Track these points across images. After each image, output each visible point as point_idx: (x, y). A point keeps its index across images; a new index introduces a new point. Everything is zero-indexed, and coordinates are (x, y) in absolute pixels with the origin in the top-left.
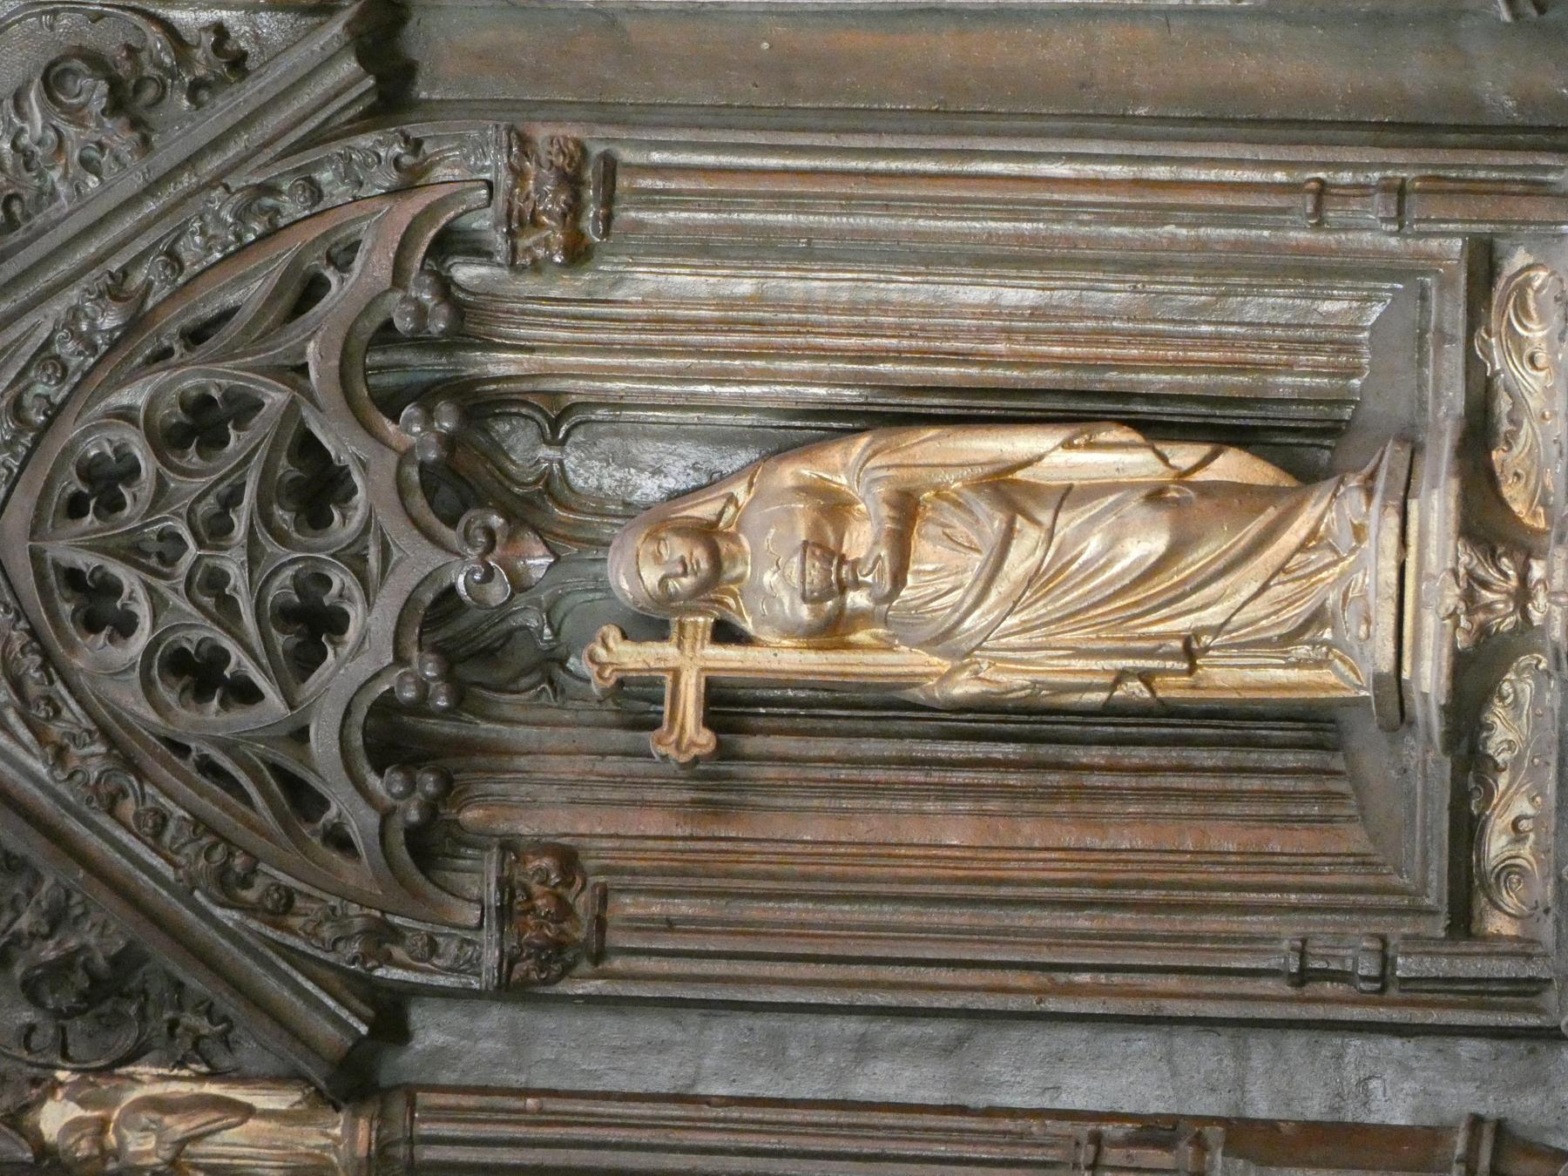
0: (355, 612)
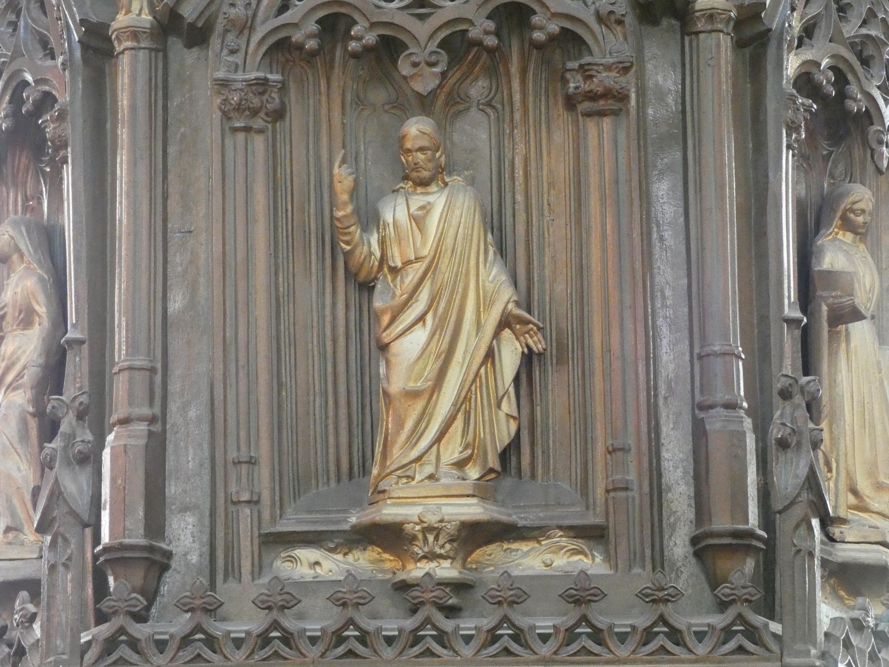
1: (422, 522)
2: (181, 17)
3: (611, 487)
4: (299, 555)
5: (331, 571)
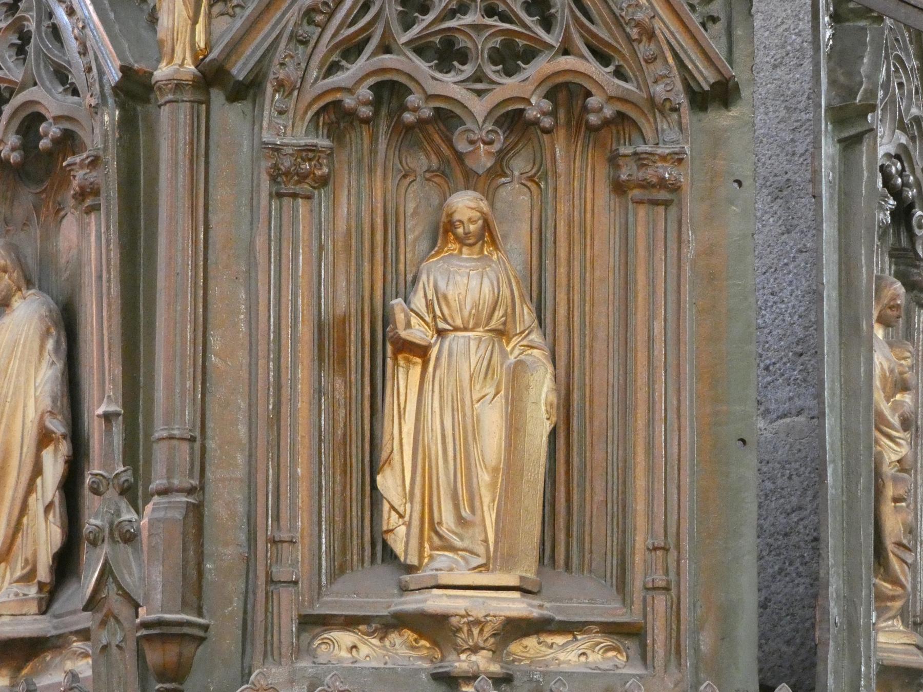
0: (449, 78)
1: (469, 615)
2: (228, 73)
3: (650, 585)
4: (337, 638)
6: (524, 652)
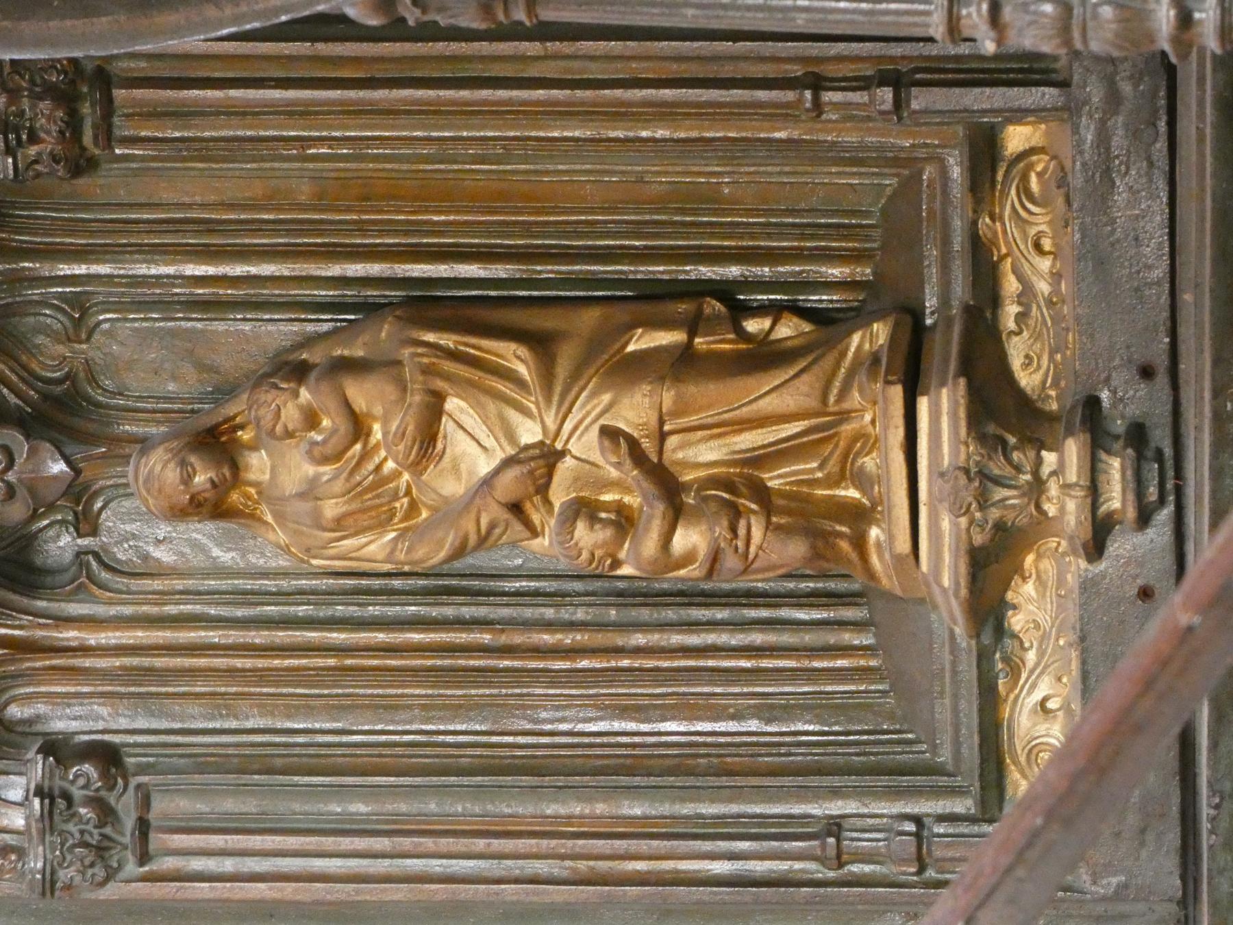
5: (1059, 679)
6: (1039, 367)
